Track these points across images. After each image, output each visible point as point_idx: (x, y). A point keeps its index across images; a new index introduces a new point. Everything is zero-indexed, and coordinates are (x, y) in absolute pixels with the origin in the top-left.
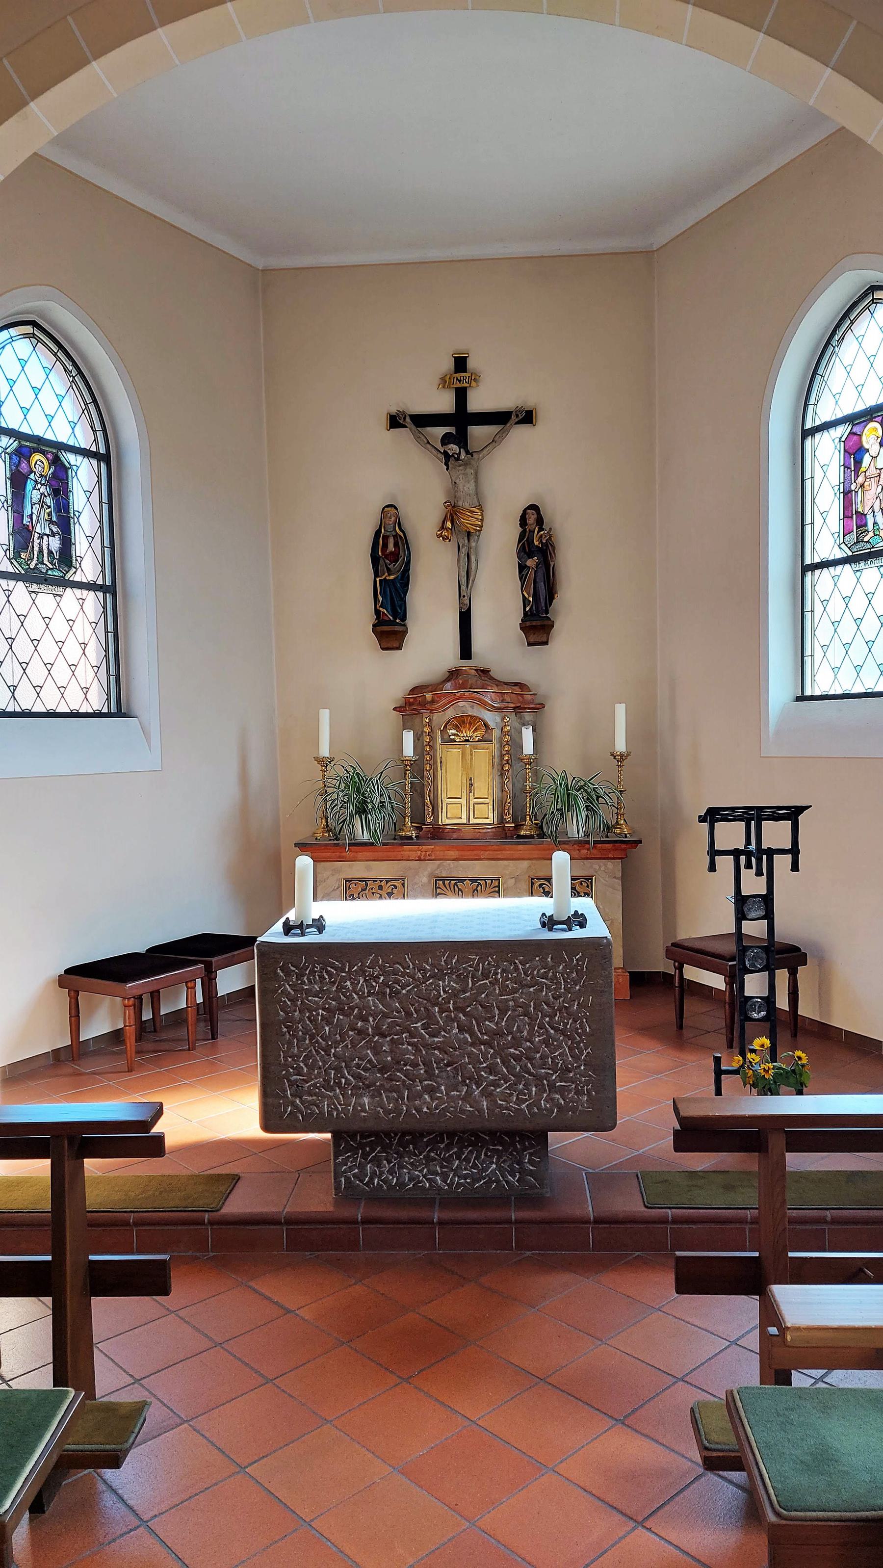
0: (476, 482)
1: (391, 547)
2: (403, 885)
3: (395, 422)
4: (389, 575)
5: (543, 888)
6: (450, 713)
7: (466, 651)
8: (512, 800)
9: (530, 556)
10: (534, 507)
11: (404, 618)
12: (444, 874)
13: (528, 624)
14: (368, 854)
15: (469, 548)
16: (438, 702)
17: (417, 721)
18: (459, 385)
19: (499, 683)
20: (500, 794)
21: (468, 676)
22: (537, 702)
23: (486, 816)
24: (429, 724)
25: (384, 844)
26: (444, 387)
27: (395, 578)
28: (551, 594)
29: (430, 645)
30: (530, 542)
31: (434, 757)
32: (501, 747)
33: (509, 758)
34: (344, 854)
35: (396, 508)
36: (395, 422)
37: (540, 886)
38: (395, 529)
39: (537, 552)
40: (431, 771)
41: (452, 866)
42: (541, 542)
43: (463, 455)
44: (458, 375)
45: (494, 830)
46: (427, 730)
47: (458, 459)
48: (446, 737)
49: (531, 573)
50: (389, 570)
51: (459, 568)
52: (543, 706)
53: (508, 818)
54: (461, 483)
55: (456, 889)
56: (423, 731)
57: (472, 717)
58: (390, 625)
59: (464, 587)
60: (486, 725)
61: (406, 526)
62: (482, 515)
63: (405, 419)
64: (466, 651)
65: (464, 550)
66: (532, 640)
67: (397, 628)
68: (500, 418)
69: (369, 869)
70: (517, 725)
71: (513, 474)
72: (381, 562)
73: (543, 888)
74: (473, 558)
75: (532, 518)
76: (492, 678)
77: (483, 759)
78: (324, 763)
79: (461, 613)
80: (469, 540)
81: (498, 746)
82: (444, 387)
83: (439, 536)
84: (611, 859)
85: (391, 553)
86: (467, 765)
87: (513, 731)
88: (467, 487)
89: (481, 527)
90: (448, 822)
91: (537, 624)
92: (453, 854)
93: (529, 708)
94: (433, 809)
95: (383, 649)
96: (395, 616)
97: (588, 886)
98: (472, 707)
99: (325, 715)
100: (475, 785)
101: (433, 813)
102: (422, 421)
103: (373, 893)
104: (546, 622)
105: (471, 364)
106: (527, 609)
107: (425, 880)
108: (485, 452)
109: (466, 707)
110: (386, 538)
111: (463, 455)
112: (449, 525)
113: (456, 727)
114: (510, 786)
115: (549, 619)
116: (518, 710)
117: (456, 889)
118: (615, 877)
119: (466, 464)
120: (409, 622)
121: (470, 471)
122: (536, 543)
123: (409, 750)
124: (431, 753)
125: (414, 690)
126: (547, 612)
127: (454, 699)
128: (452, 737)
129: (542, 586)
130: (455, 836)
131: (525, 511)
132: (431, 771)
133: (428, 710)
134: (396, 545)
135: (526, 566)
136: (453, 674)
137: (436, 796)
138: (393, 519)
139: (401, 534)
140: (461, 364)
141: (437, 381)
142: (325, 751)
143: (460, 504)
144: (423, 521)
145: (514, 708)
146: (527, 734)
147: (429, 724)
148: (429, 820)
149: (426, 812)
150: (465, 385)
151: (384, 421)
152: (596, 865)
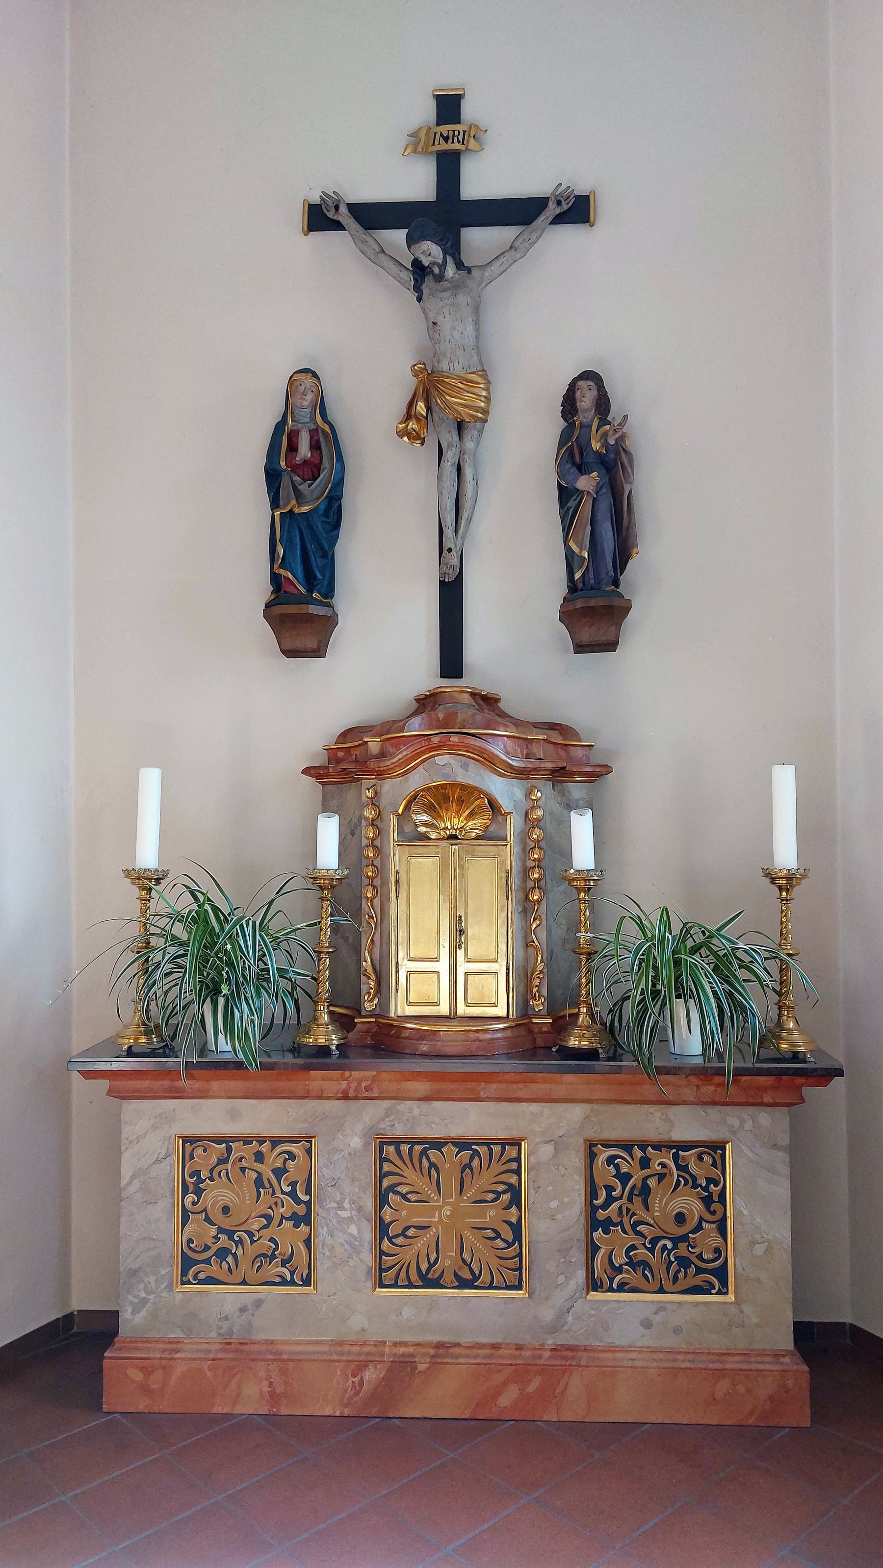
0: (477, 323)
1: (304, 451)
2: (309, 1151)
3: (319, 218)
4: (300, 504)
5: (617, 1167)
6: (418, 780)
7: (451, 661)
8: (548, 966)
9: (582, 469)
10: (589, 376)
11: (329, 592)
12: (399, 1131)
13: (579, 604)
14: (232, 1084)
15: (462, 453)
16: (393, 755)
17: (350, 793)
18: (444, 146)
19: (518, 724)
20: (521, 951)
21: (455, 705)
22: (593, 761)
23: (492, 995)
24: (374, 802)
25: (264, 1067)
26: (415, 151)
28: (624, 553)
29: (381, 650)
30: (584, 447)
31: (381, 871)
32: (526, 851)
33: (541, 882)
34: (178, 1084)
35: (315, 375)
36: (319, 218)
37: (610, 1160)
39: (595, 464)
40: (377, 902)
41: (416, 1112)
42: (606, 445)
43: (451, 271)
44: (445, 129)
45: (509, 1033)
47: (440, 278)
48: (408, 829)
49: (586, 506)
50: (299, 495)
51: (440, 493)
52: (607, 769)
53: (539, 1006)
54: (446, 323)
55: (425, 1163)
56: (361, 817)
57: (464, 787)
58: (301, 600)
59: (449, 532)
60: (493, 805)
61: (336, 414)
62: (487, 390)
63: (337, 208)
64: (451, 661)
65: (450, 456)
67: (313, 609)
68: (520, 212)
69: (234, 1115)
70: (557, 808)
71: (545, 319)
72: (285, 481)
73: (617, 1167)
74: (468, 473)
75: (586, 399)
76: (503, 715)
77: (486, 878)
78: (147, 882)
79: (442, 583)
80: (460, 436)
81: (517, 849)
82: (415, 151)
83: (401, 434)
84: (766, 1105)
85: (305, 462)
86: (453, 888)
87: (548, 819)
88: (456, 330)
89: (486, 412)
90: (410, 1011)
91: (595, 608)
92: (422, 1087)
93: (581, 774)
94: (379, 982)
95: (290, 653)
96: (310, 581)
97: (714, 1164)
98: (465, 767)
99: (151, 782)
100: (470, 932)
101: (378, 991)
102: (373, 216)
103: (243, 1170)
104: (616, 602)
105: (469, 110)
106: (577, 576)
107: (356, 1142)
108: (495, 267)
109: (450, 768)
110: (293, 437)
111: (451, 271)
112: (421, 407)
113: (430, 809)
114: (543, 936)
115: (621, 596)
116: (559, 775)
117: (425, 1163)
118: (775, 1146)
119: (456, 287)
120: (342, 601)
121: (463, 299)
122: (596, 445)
123: (328, 856)
124: (377, 862)
125: (346, 735)
126: (616, 583)
127: (427, 747)
129: (607, 531)
130: (424, 1048)
131: (572, 387)
132: (377, 902)
133: (371, 772)
134: (315, 446)
136: (426, 703)
137: (385, 957)
138: (310, 397)
139: (327, 429)
140: (448, 107)
141: (404, 140)
142: (148, 856)
143: (444, 365)
144: (369, 407)
145: (553, 772)
146: (582, 826)
147: (374, 802)
148: (368, 1007)
149: (364, 988)
150: (457, 146)
151: (299, 217)
152: (735, 1117)
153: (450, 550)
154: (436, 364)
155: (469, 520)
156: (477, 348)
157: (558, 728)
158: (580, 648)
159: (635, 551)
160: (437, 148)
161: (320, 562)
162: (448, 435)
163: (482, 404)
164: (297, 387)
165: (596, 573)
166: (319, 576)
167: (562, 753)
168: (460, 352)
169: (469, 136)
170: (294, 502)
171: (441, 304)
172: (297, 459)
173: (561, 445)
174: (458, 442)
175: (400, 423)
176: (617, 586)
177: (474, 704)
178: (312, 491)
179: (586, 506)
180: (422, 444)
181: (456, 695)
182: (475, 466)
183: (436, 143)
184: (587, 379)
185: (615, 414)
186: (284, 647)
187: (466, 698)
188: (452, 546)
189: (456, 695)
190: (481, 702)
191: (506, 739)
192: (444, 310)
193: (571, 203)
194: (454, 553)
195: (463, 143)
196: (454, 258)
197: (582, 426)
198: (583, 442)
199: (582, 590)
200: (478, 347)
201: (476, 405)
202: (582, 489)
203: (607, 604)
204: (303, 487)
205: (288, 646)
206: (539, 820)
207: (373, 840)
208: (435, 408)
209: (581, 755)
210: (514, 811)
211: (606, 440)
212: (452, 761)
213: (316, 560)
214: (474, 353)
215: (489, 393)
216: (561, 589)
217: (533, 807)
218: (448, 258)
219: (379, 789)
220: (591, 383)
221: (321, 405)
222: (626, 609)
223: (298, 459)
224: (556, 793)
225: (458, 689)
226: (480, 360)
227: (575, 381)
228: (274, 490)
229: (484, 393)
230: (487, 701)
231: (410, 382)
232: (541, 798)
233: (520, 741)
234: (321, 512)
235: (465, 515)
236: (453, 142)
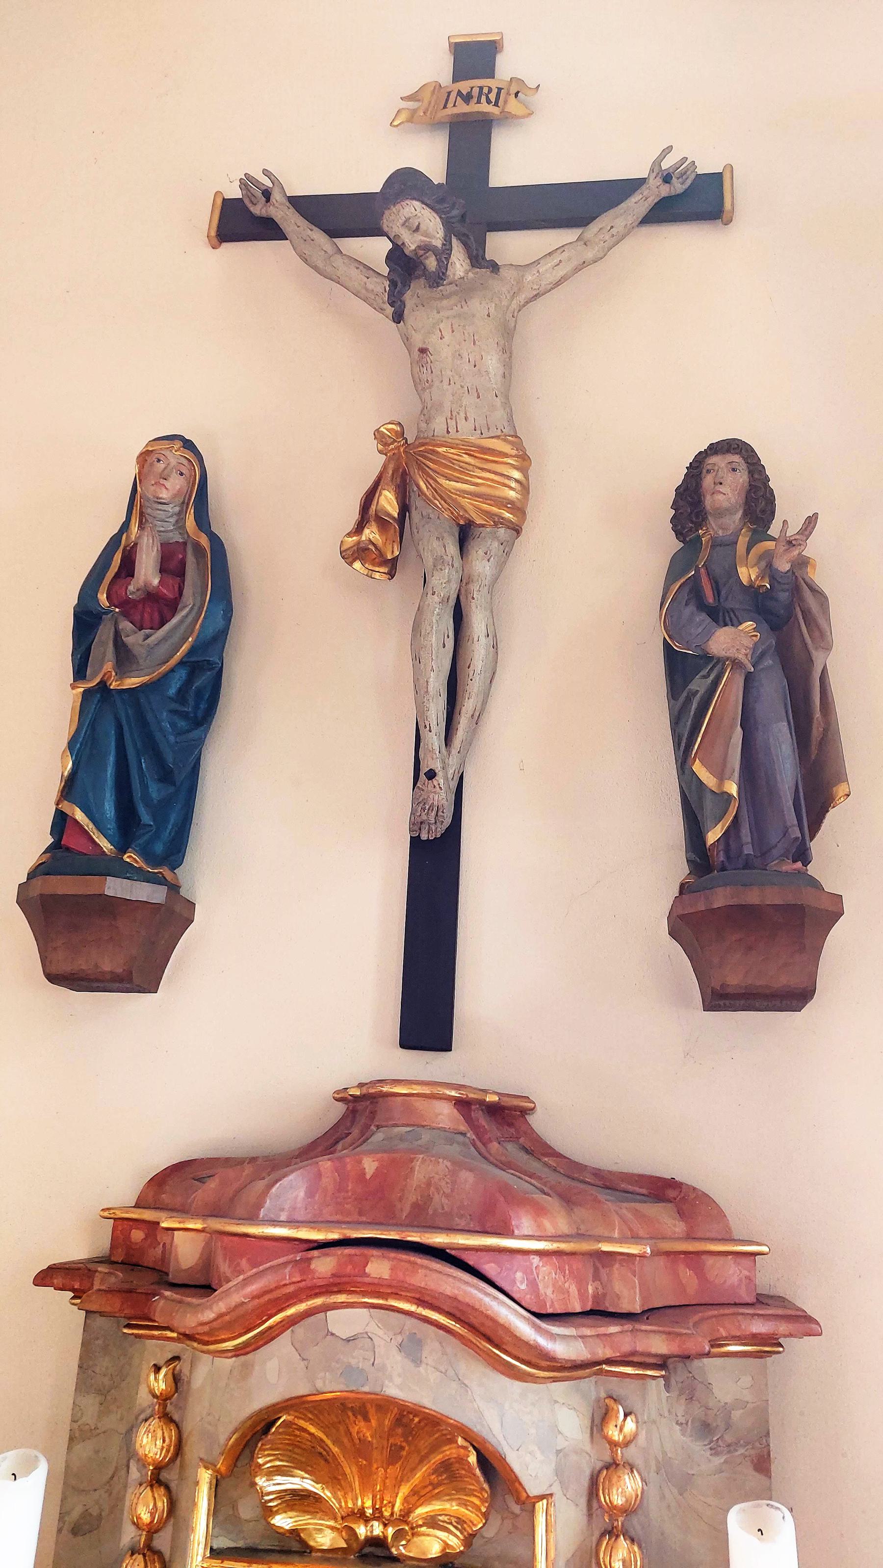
1: (147, 572)
3: (242, 221)
6: (278, 1374)
7: (427, 1012)
9: (720, 616)
13: (721, 898)
15: (465, 582)
18: (463, 108)
24: (168, 1410)
27: (143, 687)
28: (818, 792)
29: (271, 998)
35: (188, 445)
36: (242, 221)
38: (180, 524)
42: (769, 571)
43: (459, 264)
44: (464, 86)
46: (151, 1443)
47: (437, 279)
49: (730, 692)
50: (125, 658)
54: (444, 349)
58: (113, 893)
59: (434, 739)
60: (491, 1466)
64: (427, 1012)
66: (734, 978)
67: (115, 887)
72: (104, 633)
74: (478, 623)
76: (540, 1149)
79: (415, 842)
85: (151, 596)
89: (519, 509)
96: (127, 829)
98: (411, 1348)
104: (808, 898)
105: (507, 67)
106: (713, 836)
109: (372, 1348)
111: (459, 264)
112: (388, 502)
115: (815, 884)
119: (465, 290)
122: (747, 574)
125: (176, 1182)
126: (803, 855)
128: (283, 1521)
131: (696, 469)
135: (707, 658)
136: (362, 1109)
143: (438, 426)
144: (290, 518)
150: (484, 107)
153: (431, 775)
154: (423, 425)
155: (477, 719)
156: (506, 396)
157: (671, 1193)
158: (718, 999)
159: (841, 789)
160: (451, 111)
161: (155, 791)
162: (435, 544)
163: (512, 494)
164: (152, 465)
165: (758, 829)
166: (146, 818)
167: (687, 1274)
168: (469, 400)
169: (508, 94)
170: (109, 666)
171: (437, 316)
172: (131, 588)
173: (672, 574)
174: (457, 562)
175: (349, 535)
176: (806, 861)
177: (463, 1127)
178: (151, 649)
179: (730, 692)
180: (391, 575)
181: (419, 1104)
182: (492, 613)
183: (450, 104)
184: (728, 451)
185: (788, 514)
186: (53, 970)
187: (445, 1114)
188: (437, 766)
189: (419, 1104)
190: (483, 1120)
191: (536, 1260)
192: (442, 326)
193: (689, 182)
194: (440, 779)
195: (496, 104)
196: (466, 245)
197: (716, 544)
198: (718, 571)
199: (723, 869)
200: (507, 397)
201: (497, 493)
202: (723, 654)
203: (790, 899)
204: (134, 639)
205: (65, 967)
206: (628, 1511)
207: (152, 1531)
208: (416, 503)
209: (735, 1280)
210: (556, 1489)
211: (770, 565)
212: (373, 1328)
213: (145, 787)
214: (498, 402)
215: (526, 477)
216: (675, 867)
217: (612, 1466)
218: (454, 241)
219: (186, 1371)
220: (736, 458)
221: (200, 497)
222: (831, 912)
223: (132, 588)
224: (674, 1394)
225: (426, 1090)
226: (511, 420)
227: (700, 459)
228: (83, 648)
229: (517, 475)
230: (500, 1117)
231: (374, 462)
232: (635, 1436)
233: (577, 1264)
234: (172, 691)
235: (468, 706)
236: (479, 102)
